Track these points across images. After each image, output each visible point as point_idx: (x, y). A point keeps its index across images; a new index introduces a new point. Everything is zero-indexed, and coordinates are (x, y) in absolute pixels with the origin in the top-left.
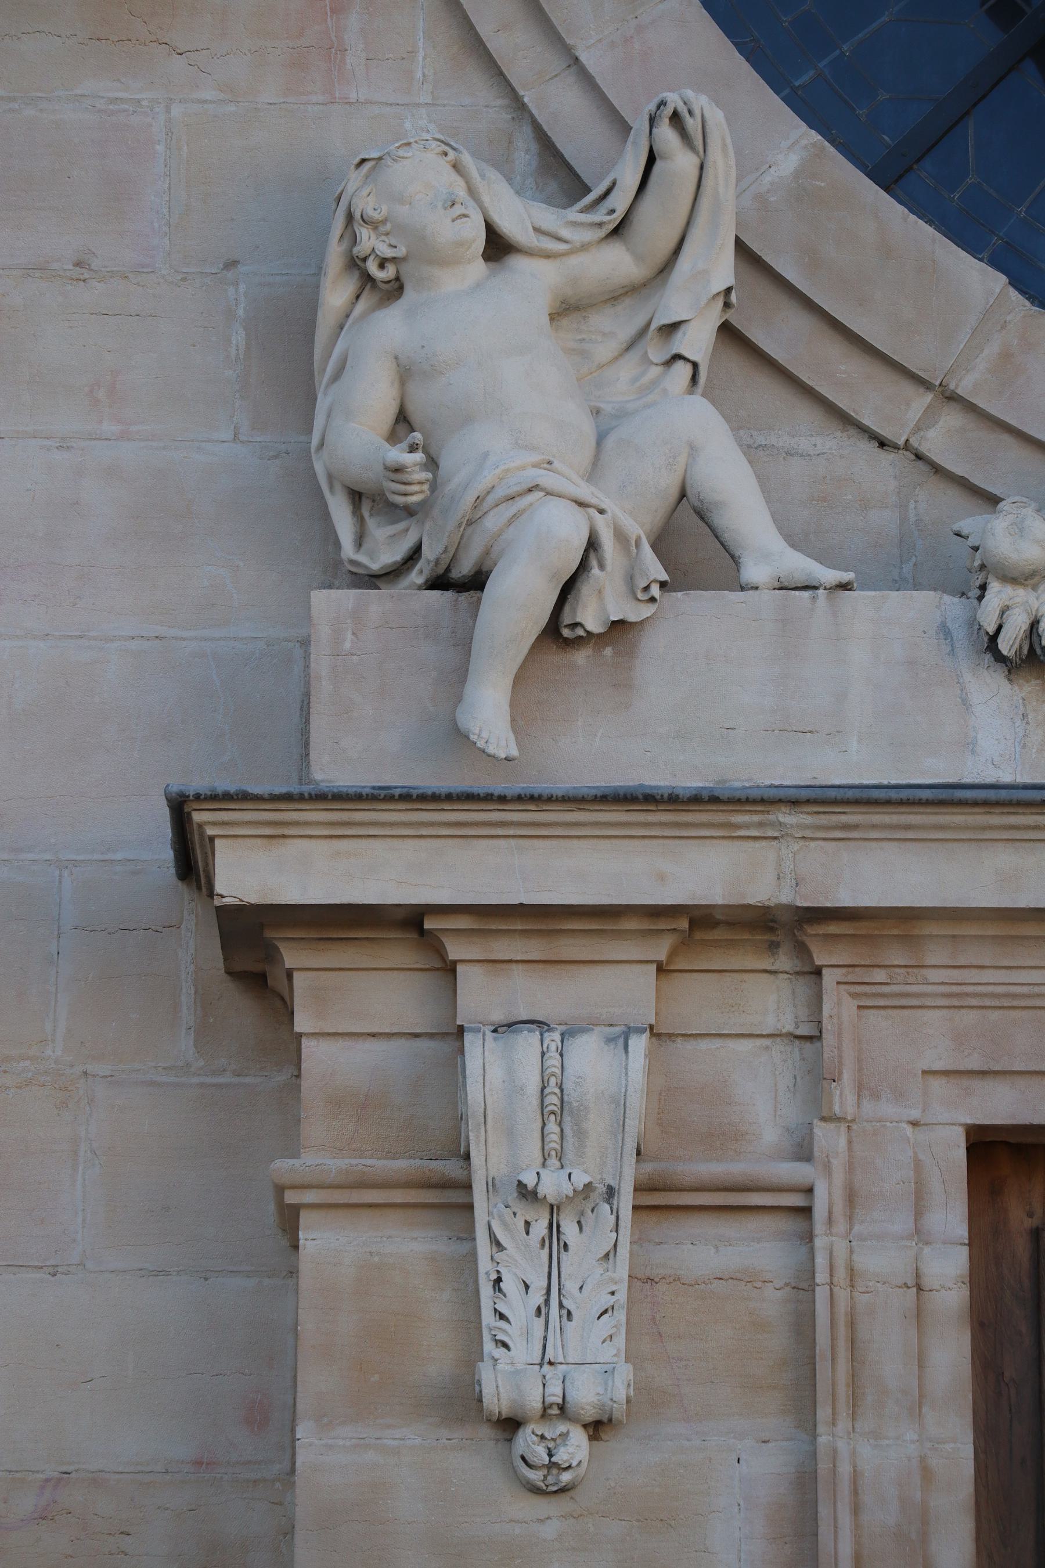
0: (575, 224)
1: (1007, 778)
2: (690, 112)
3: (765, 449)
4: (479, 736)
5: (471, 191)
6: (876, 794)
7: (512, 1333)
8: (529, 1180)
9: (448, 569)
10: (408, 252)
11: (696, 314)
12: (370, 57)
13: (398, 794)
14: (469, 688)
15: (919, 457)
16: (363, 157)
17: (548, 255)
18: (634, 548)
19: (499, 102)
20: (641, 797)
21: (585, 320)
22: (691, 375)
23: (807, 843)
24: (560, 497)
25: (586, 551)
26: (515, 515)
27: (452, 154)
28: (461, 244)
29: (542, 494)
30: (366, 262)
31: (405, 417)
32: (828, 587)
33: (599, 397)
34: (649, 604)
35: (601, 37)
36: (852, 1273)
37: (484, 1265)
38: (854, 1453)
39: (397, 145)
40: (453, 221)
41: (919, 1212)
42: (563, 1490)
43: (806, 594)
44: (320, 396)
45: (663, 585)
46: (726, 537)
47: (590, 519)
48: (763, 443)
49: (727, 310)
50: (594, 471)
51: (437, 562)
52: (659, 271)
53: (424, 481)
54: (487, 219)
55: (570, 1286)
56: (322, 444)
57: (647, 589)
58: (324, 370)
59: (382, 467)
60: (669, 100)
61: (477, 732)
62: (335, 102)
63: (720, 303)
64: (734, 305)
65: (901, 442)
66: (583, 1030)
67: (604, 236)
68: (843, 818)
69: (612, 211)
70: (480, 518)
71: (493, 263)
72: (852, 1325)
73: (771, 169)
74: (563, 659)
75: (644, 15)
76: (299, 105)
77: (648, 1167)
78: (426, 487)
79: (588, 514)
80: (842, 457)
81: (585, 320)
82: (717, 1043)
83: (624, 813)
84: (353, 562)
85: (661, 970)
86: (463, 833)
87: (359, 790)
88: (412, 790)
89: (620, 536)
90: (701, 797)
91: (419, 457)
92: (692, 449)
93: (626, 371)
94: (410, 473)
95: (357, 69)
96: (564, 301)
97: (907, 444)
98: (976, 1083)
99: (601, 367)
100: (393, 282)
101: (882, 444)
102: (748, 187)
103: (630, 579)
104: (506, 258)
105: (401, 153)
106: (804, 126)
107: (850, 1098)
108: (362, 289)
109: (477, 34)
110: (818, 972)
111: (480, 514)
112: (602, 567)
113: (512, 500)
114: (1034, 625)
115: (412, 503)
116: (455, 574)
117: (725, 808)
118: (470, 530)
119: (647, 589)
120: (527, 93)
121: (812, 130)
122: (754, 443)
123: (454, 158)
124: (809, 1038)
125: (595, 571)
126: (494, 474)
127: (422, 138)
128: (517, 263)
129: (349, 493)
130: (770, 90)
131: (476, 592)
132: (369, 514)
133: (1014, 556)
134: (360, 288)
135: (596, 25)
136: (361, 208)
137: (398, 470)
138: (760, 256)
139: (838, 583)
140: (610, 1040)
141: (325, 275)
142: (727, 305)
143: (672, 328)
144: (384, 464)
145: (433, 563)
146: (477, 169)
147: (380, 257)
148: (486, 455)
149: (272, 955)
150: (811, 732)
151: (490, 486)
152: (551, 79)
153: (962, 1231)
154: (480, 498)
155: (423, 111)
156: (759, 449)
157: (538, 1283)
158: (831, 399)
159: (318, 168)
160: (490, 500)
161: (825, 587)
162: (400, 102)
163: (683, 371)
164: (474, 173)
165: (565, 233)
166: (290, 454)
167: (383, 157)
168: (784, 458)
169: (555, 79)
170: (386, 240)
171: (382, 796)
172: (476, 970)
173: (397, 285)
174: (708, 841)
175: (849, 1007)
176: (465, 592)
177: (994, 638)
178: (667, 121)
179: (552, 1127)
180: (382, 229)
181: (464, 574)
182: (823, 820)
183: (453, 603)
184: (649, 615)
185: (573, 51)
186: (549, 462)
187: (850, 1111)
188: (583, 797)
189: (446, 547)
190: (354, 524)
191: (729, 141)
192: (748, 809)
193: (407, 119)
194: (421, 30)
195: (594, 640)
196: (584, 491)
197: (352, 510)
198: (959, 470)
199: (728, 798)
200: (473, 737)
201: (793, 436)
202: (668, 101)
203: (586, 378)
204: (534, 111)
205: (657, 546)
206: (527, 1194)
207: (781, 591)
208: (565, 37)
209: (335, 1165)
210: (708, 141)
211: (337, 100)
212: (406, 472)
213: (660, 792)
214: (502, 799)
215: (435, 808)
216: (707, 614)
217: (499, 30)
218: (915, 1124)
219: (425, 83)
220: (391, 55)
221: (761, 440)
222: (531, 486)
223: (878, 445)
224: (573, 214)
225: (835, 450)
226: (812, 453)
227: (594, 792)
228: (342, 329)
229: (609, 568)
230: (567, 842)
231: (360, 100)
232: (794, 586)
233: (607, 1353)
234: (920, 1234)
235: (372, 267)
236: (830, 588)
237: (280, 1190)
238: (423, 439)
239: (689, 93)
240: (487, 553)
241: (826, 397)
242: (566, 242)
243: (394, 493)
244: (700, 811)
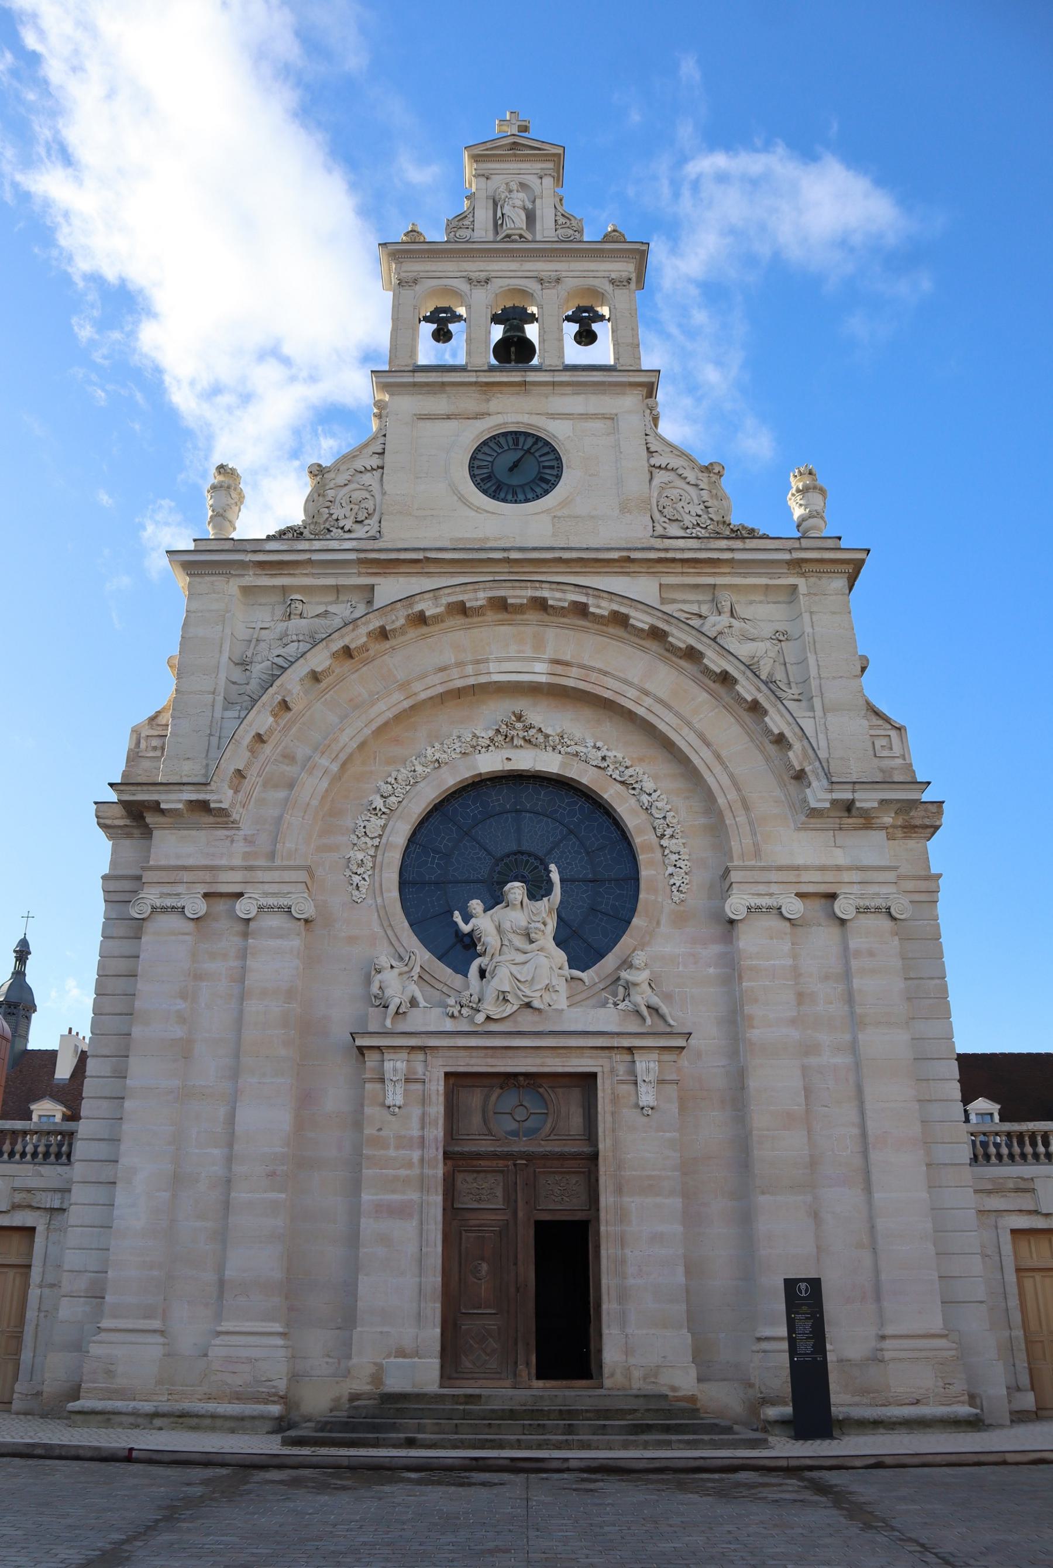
6: (155, 1456)
50: (402, 994)
86: (384, 1037)
143: (412, 977)
196: (401, 996)
206: (391, 1080)
209: (369, 1076)
234: (438, 1085)
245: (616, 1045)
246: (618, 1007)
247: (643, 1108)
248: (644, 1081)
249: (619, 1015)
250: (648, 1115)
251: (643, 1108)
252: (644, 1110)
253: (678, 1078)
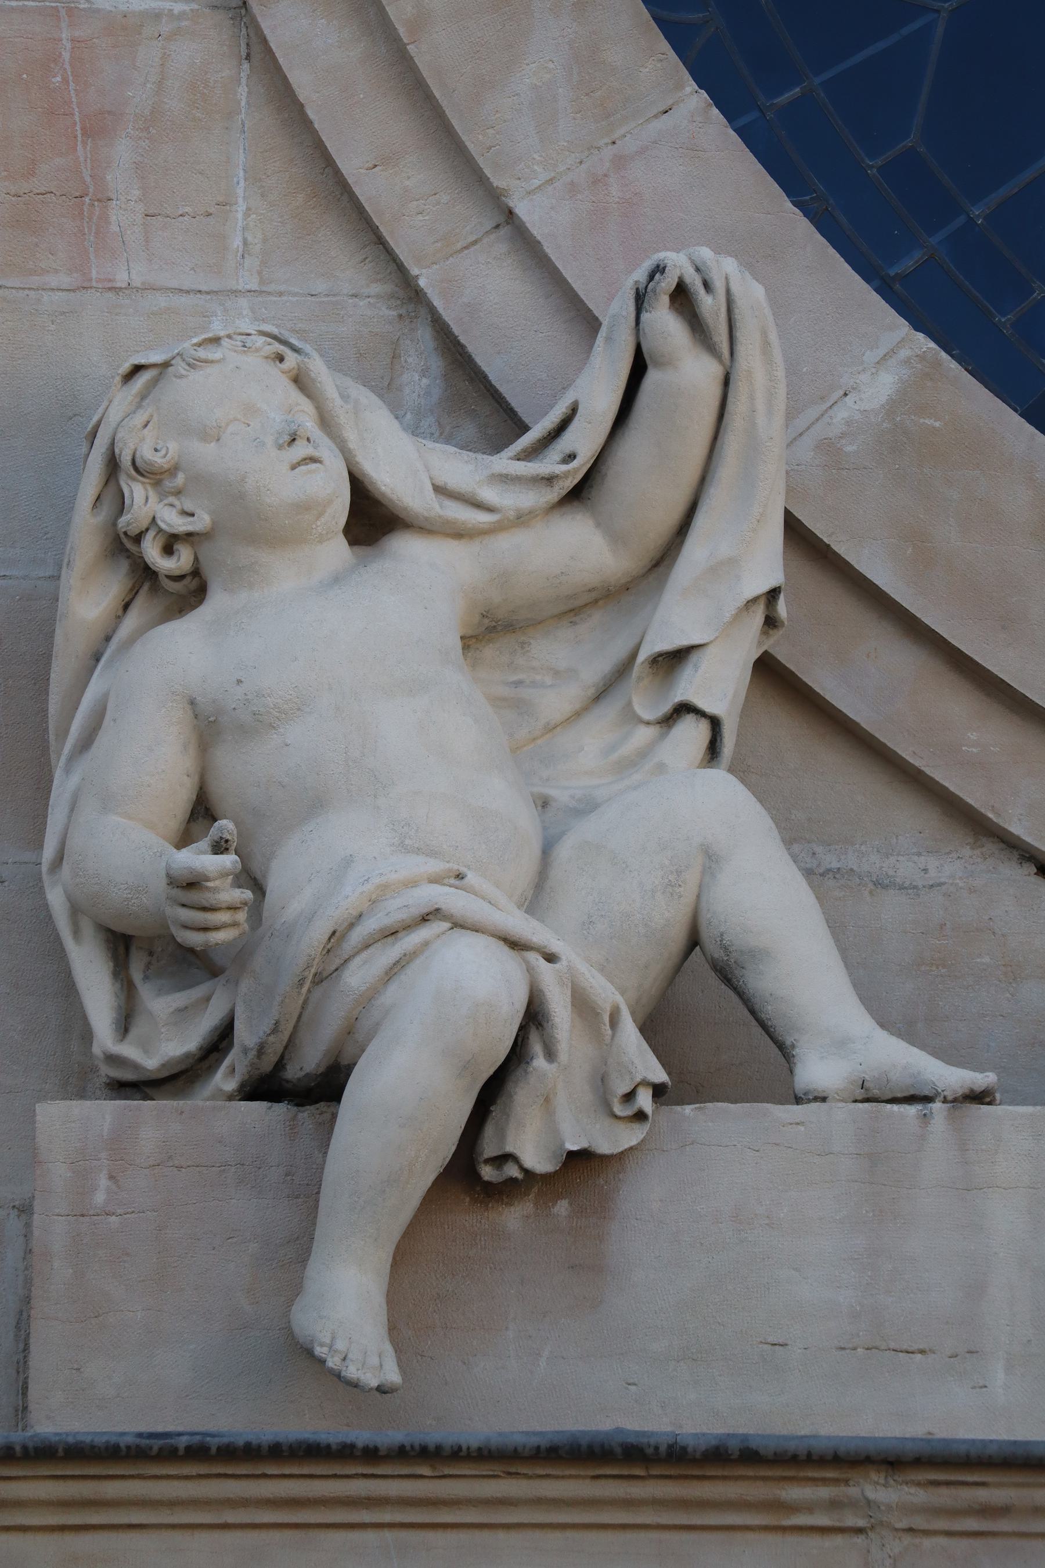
0: (505, 479)
2: (707, 285)
3: (837, 876)
4: (330, 1347)
5: (326, 422)
9: (280, 1065)
10: (214, 523)
11: (717, 634)
12: (151, 212)
13: (184, 1445)
16: (136, 362)
17: (459, 533)
18: (608, 1027)
19: (376, 288)
20: (618, 1450)
21: (523, 648)
22: (707, 741)
23: (917, 1541)
24: (477, 931)
25: (523, 1029)
26: (398, 962)
27: (291, 359)
28: (305, 507)
29: (446, 925)
30: (140, 544)
31: (207, 809)
32: (950, 1098)
33: (548, 780)
34: (633, 1124)
35: (553, 175)
39: (195, 340)
40: (293, 468)
43: (912, 1110)
44: (58, 774)
45: (659, 1091)
46: (769, 1011)
47: (530, 970)
48: (835, 865)
49: (771, 632)
51: (261, 1050)
52: (654, 562)
53: (239, 906)
54: (355, 471)
57: (629, 1097)
58: (67, 731)
59: (164, 881)
60: (669, 263)
61: (328, 1341)
62: (91, 288)
63: (758, 617)
64: (783, 623)
67: (556, 499)
68: (982, 1495)
69: (570, 456)
70: (336, 970)
71: (364, 547)
73: (847, 399)
74: (483, 1221)
75: (626, 138)
76: (27, 292)
78: (241, 916)
79: (527, 963)
80: (972, 890)
81: (523, 648)
83: (588, 1481)
84: (113, 1059)
87: (114, 1439)
88: (208, 1439)
90: (727, 1451)
91: (229, 860)
92: (710, 857)
94: (215, 890)
95: (129, 232)
96: (488, 612)
99: (550, 729)
100: (188, 579)
102: (808, 428)
103: (601, 1081)
104: (386, 539)
105: (202, 353)
106: (903, 326)
108: (134, 592)
109: (337, 172)
111: (338, 962)
113: (393, 937)
115: (217, 944)
116: (293, 1072)
117: (769, 1473)
118: (318, 992)
119: (629, 1097)
120: (424, 271)
121: (918, 333)
122: (819, 865)
123: (296, 366)
125: (539, 1062)
126: (362, 893)
127: (239, 331)
129: (108, 941)
130: (846, 265)
131: (329, 1103)
132: (142, 976)
134: (131, 590)
135: (543, 154)
136: (133, 447)
137: (192, 883)
138: (829, 546)
139: (967, 1091)
141: (68, 564)
142: (771, 622)
144: (168, 875)
145: (254, 1052)
146: (336, 386)
147: (165, 532)
148: (348, 862)
150: (922, 1352)
151: (355, 913)
152: (466, 248)
154: (337, 934)
155: (243, 302)
156: (828, 876)
158: (952, 789)
159: (60, 398)
160: (356, 936)
161: (945, 1097)
162: (204, 288)
165: (489, 494)
166: (6, 884)
167: (173, 362)
168: (871, 892)
169: (472, 249)
170: (177, 503)
171: (155, 1449)
173: (194, 584)
174: (738, 1536)
176: (310, 1104)
178: (665, 299)
180: (168, 484)
181: (308, 1071)
182: (944, 1496)
183: (288, 1123)
184: (634, 1142)
185: (504, 199)
186: (458, 876)
188: (516, 1449)
189: (277, 1023)
190: (116, 993)
191: (773, 337)
192: (810, 1474)
193: (216, 316)
194: (241, 167)
195: (536, 1187)
197: (111, 969)
199: (775, 1454)
200: (319, 1351)
201: (887, 856)
202: (668, 265)
203: (525, 748)
204: (437, 303)
205: (649, 1029)
207: (866, 1105)
208: (489, 175)
210: (739, 334)
211: (94, 284)
212: (207, 888)
213: (652, 1441)
214: (371, 1454)
215: (250, 1473)
216: (735, 1143)
217: (376, 166)
219: (246, 256)
220: (187, 209)
221: (831, 861)
222: (426, 910)
223: (1035, 870)
224: (504, 462)
225: (961, 878)
226: (920, 884)
227: (534, 1441)
228: (98, 660)
229: (563, 1056)
230: (486, 1535)
231: (133, 284)
232: (889, 1096)
235: (152, 551)
236: (955, 1100)
238: (238, 833)
239: (705, 253)
240: (349, 1031)
241: (944, 787)
242: (489, 509)
243: (186, 927)
244: (725, 1478)
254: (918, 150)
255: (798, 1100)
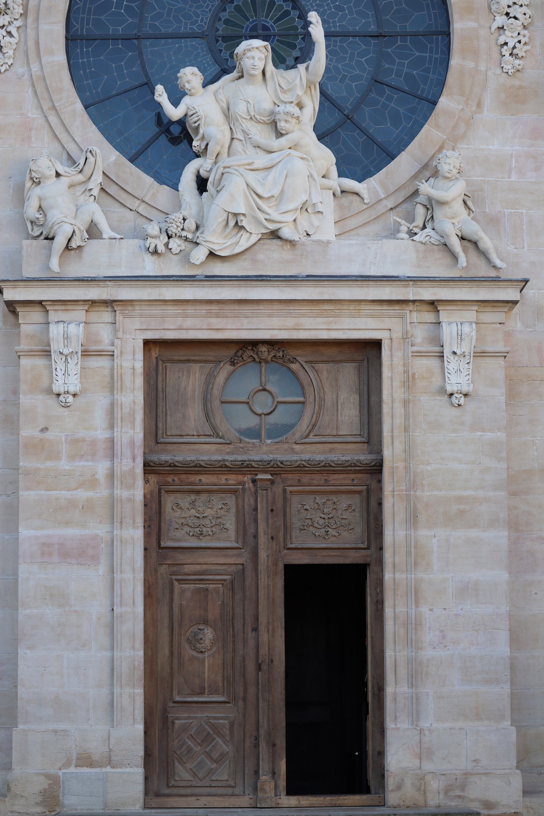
0: (72, 171)
1: (151, 274)
5: (53, 165)
7: (58, 378)
8: (61, 351)
14: (51, 259)
15: (138, 212)
17: (67, 177)
27: (49, 158)
36: (121, 366)
37: (54, 366)
38: (121, 399)
41: (134, 355)
42: (68, 406)
43: (114, 240)
45: (88, 239)
46: (100, 229)
50: (75, 218)
55: (69, 370)
56: (25, 212)
63: (100, 185)
65: (134, 210)
66: (72, 323)
72: (121, 376)
77: (84, 348)
82: (97, 324)
85: (86, 311)
86: (49, 286)
89: (79, 229)
93: (82, 198)
97: (135, 210)
98: (145, 331)
101: (131, 210)
103: (82, 238)
107: (121, 335)
110: (116, 311)
112: (76, 236)
114: (156, 246)
124: (114, 323)
125: (74, 237)
128: (61, 178)
133: (152, 233)
137: (38, 218)
140: (76, 325)
142: (101, 185)
148: (54, 215)
149: (15, 309)
153: (142, 358)
157: (63, 369)
160: (55, 224)
163: (93, 198)
164: (54, 162)
165: (70, 172)
172: (52, 311)
175: (121, 318)
177: (148, 248)
179: (66, 341)
187: (121, 337)
196: (73, 222)
198: (145, 215)
205: (87, 232)
206: (61, 353)
209: (26, 348)
218: (133, 339)
224: (72, 169)
233: (76, 382)
234: (134, 359)
235: (35, 179)
237: (17, 352)
239: (93, 147)
240: (55, 233)
245: (411, 299)
246: (415, 238)
247: (452, 394)
248: (454, 353)
249: (417, 251)
250: (459, 405)
251: (452, 394)
252: (453, 398)
253: (507, 349)
254: (181, 32)
255: (103, 239)
